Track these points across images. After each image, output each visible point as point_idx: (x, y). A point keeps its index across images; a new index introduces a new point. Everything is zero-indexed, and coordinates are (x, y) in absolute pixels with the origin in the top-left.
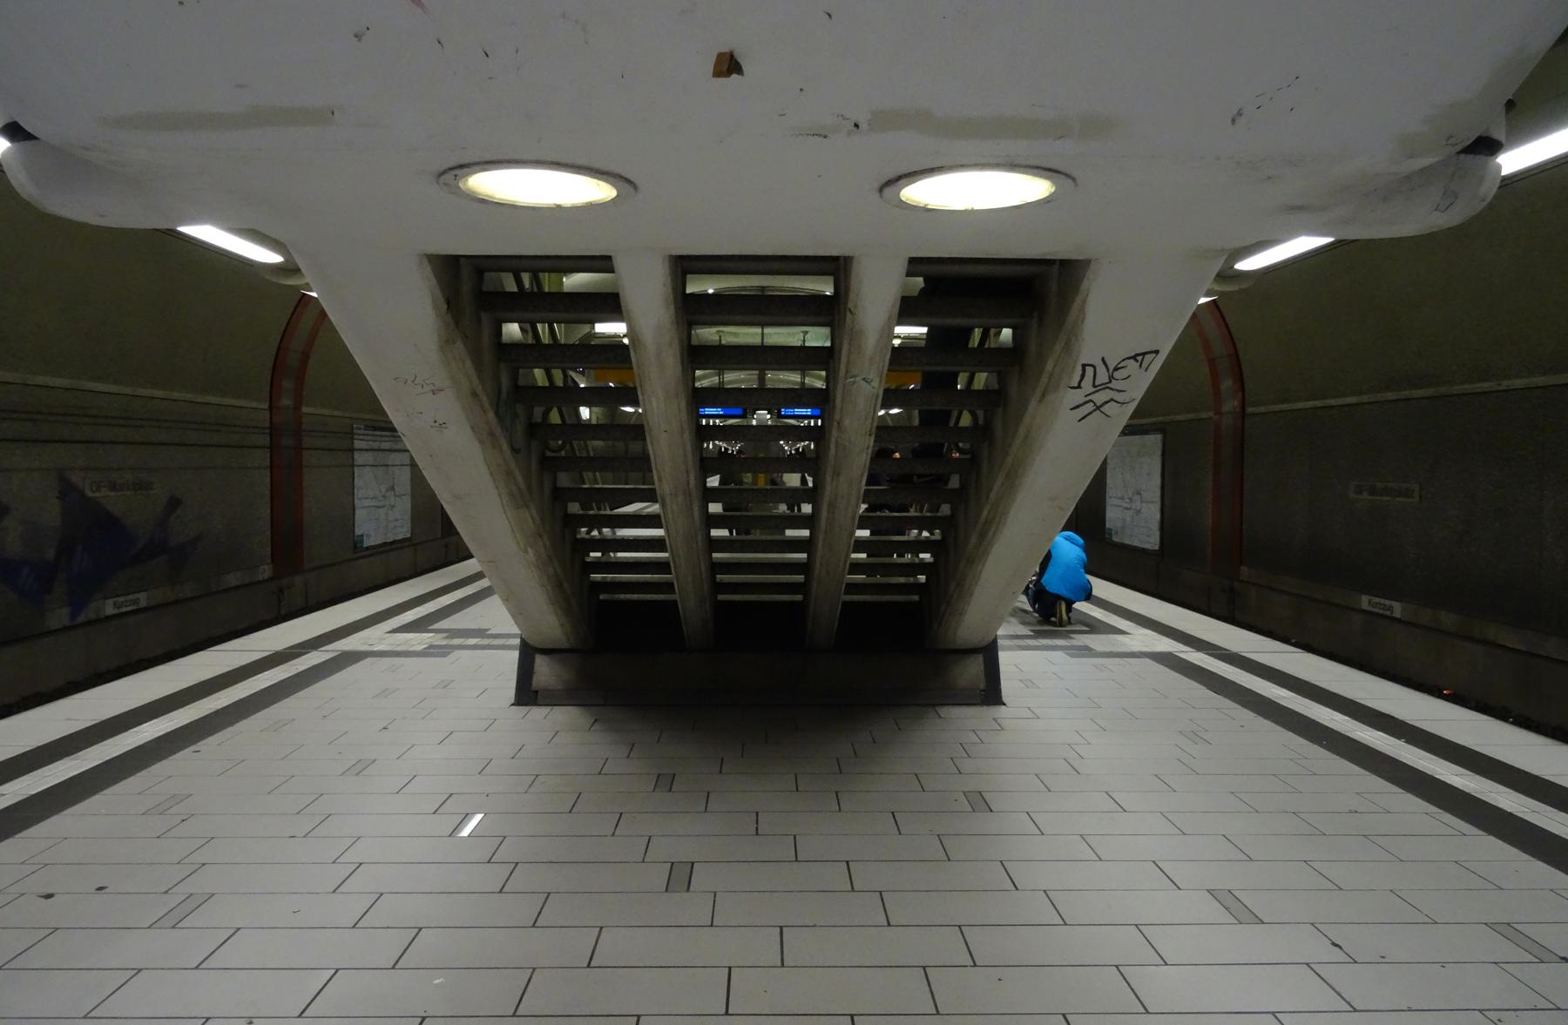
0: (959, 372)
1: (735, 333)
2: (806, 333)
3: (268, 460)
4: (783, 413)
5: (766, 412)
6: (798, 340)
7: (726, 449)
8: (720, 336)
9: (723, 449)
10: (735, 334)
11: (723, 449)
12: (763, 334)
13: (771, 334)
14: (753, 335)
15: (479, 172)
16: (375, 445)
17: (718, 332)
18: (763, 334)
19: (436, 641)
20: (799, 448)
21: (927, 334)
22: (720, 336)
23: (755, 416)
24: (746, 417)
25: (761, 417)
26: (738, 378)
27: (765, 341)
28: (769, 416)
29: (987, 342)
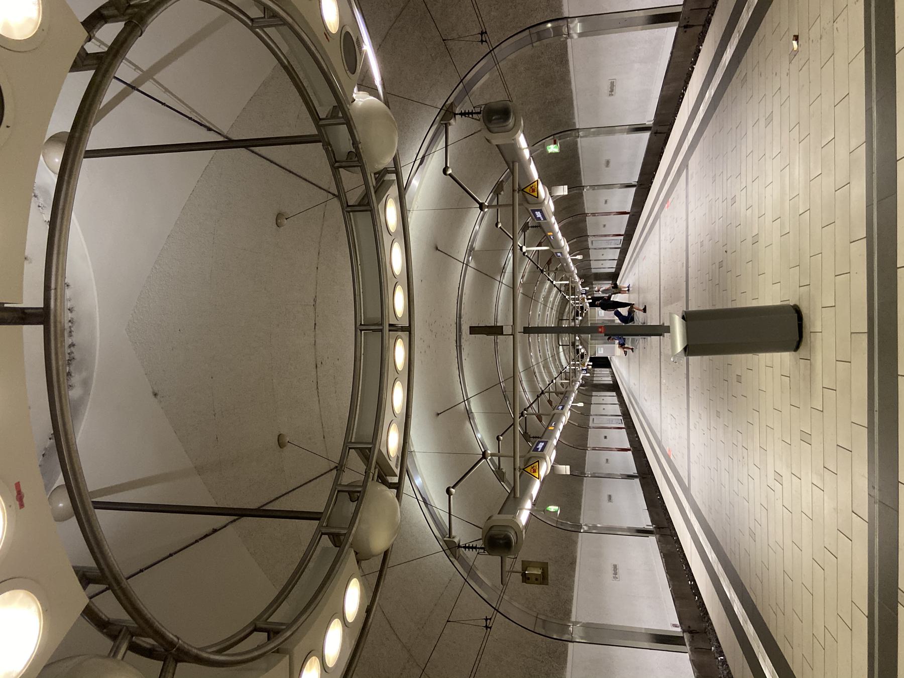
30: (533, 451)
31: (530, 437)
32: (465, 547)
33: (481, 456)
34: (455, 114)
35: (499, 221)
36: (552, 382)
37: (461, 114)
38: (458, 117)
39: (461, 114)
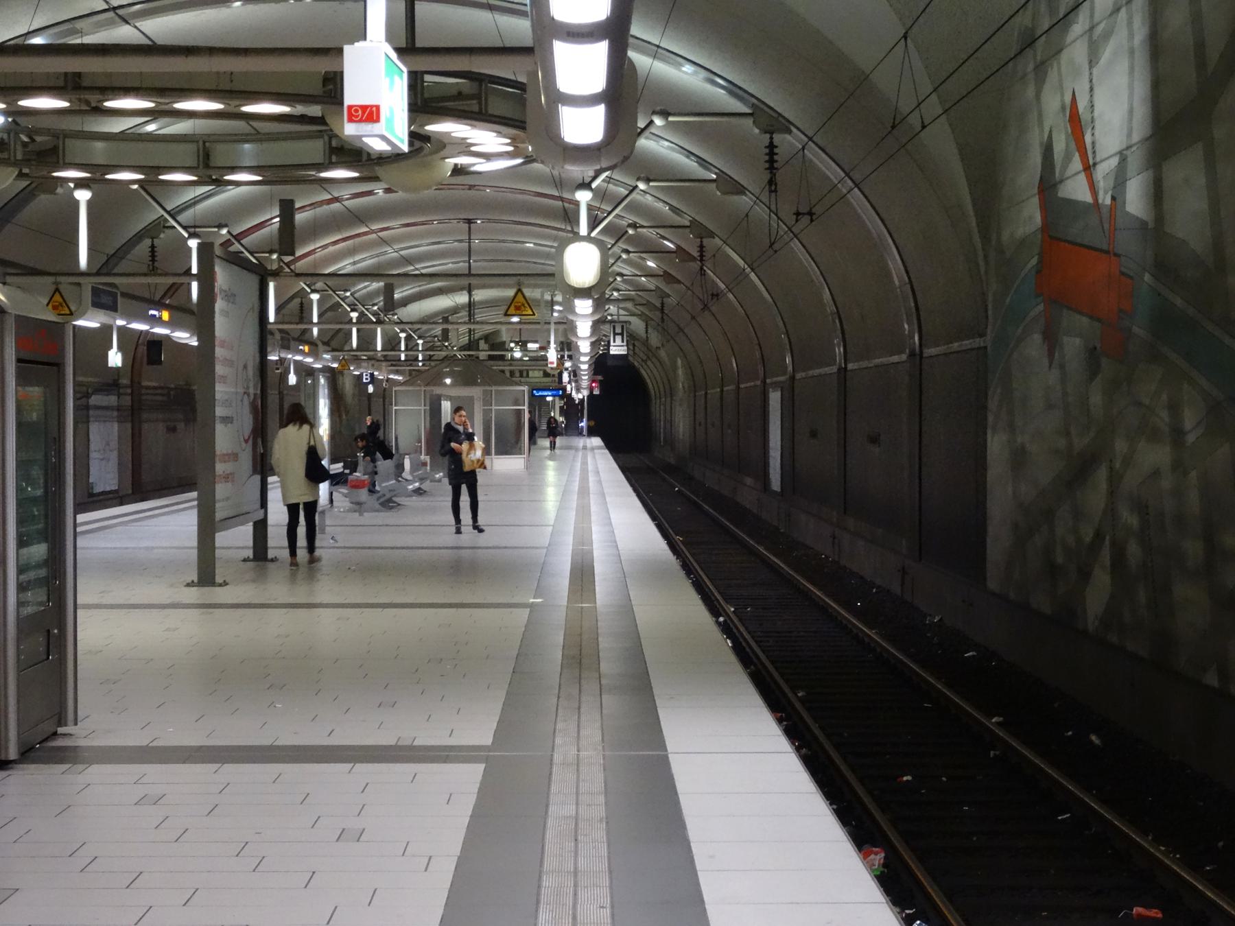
35: (625, 277)
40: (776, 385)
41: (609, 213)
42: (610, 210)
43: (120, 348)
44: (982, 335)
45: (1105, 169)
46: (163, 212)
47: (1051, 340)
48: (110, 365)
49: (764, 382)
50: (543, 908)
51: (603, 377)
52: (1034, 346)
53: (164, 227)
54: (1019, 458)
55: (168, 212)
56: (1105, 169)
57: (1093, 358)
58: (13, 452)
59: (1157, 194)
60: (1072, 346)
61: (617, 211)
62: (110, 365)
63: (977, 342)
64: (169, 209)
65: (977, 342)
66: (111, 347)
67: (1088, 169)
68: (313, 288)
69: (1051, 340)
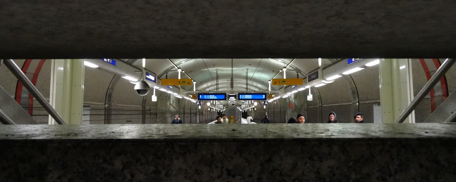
0: (148, 90)
1: (222, 70)
2: (248, 69)
3: (104, 118)
4: (240, 98)
5: (234, 98)
6: (245, 72)
7: (220, 111)
8: (217, 71)
9: (219, 111)
10: (222, 70)
11: (219, 111)
12: (232, 70)
13: (235, 70)
14: (229, 70)
15: (368, 66)
16: (61, 120)
17: (216, 69)
18: (232, 70)
19: (273, 130)
20: (245, 110)
21: (106, 59)
22: (217, 71)
23: (229, 99)
24: (226, 100)
25: (232, 100)
26: (224, 86)
27: (233, 72)
28: (235, 99)
29: (213, 71)
30: (146, 72)
31: (167, 73)
32: (167, 75)
33: (179, 67)
34: (298, 73)
36: (179, 68)
37: (298, 75)
38: (297, 73)
39: (298, 75)
40: (266, 112)
41: (289, 64)
42: (289, 63)
43: (156, 95)
44: (285, 108)
45: (292, 99)
46: (173, 65)
47: (289, 110)
48: (152, 101)
49: (265, 111)
50: (250, 96)
51: (33, 98)
52: (288, 110)
53: (170, 71)
54: (288, 118)
55: (175, 65)
56: (292, 99)
57: (292, 111)
58: (381, 97)
59: (295, 101)
60: (291, 110)
61: (291, 63)
62: (152, 101)
63: (285, 109)
64: (175, 64)
65: (285, 109)
66: (153, 94)
67: (291, 98)
68: (178, 66)
69: (289, 110)
